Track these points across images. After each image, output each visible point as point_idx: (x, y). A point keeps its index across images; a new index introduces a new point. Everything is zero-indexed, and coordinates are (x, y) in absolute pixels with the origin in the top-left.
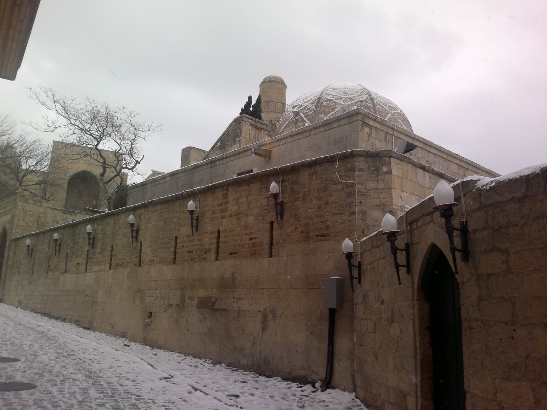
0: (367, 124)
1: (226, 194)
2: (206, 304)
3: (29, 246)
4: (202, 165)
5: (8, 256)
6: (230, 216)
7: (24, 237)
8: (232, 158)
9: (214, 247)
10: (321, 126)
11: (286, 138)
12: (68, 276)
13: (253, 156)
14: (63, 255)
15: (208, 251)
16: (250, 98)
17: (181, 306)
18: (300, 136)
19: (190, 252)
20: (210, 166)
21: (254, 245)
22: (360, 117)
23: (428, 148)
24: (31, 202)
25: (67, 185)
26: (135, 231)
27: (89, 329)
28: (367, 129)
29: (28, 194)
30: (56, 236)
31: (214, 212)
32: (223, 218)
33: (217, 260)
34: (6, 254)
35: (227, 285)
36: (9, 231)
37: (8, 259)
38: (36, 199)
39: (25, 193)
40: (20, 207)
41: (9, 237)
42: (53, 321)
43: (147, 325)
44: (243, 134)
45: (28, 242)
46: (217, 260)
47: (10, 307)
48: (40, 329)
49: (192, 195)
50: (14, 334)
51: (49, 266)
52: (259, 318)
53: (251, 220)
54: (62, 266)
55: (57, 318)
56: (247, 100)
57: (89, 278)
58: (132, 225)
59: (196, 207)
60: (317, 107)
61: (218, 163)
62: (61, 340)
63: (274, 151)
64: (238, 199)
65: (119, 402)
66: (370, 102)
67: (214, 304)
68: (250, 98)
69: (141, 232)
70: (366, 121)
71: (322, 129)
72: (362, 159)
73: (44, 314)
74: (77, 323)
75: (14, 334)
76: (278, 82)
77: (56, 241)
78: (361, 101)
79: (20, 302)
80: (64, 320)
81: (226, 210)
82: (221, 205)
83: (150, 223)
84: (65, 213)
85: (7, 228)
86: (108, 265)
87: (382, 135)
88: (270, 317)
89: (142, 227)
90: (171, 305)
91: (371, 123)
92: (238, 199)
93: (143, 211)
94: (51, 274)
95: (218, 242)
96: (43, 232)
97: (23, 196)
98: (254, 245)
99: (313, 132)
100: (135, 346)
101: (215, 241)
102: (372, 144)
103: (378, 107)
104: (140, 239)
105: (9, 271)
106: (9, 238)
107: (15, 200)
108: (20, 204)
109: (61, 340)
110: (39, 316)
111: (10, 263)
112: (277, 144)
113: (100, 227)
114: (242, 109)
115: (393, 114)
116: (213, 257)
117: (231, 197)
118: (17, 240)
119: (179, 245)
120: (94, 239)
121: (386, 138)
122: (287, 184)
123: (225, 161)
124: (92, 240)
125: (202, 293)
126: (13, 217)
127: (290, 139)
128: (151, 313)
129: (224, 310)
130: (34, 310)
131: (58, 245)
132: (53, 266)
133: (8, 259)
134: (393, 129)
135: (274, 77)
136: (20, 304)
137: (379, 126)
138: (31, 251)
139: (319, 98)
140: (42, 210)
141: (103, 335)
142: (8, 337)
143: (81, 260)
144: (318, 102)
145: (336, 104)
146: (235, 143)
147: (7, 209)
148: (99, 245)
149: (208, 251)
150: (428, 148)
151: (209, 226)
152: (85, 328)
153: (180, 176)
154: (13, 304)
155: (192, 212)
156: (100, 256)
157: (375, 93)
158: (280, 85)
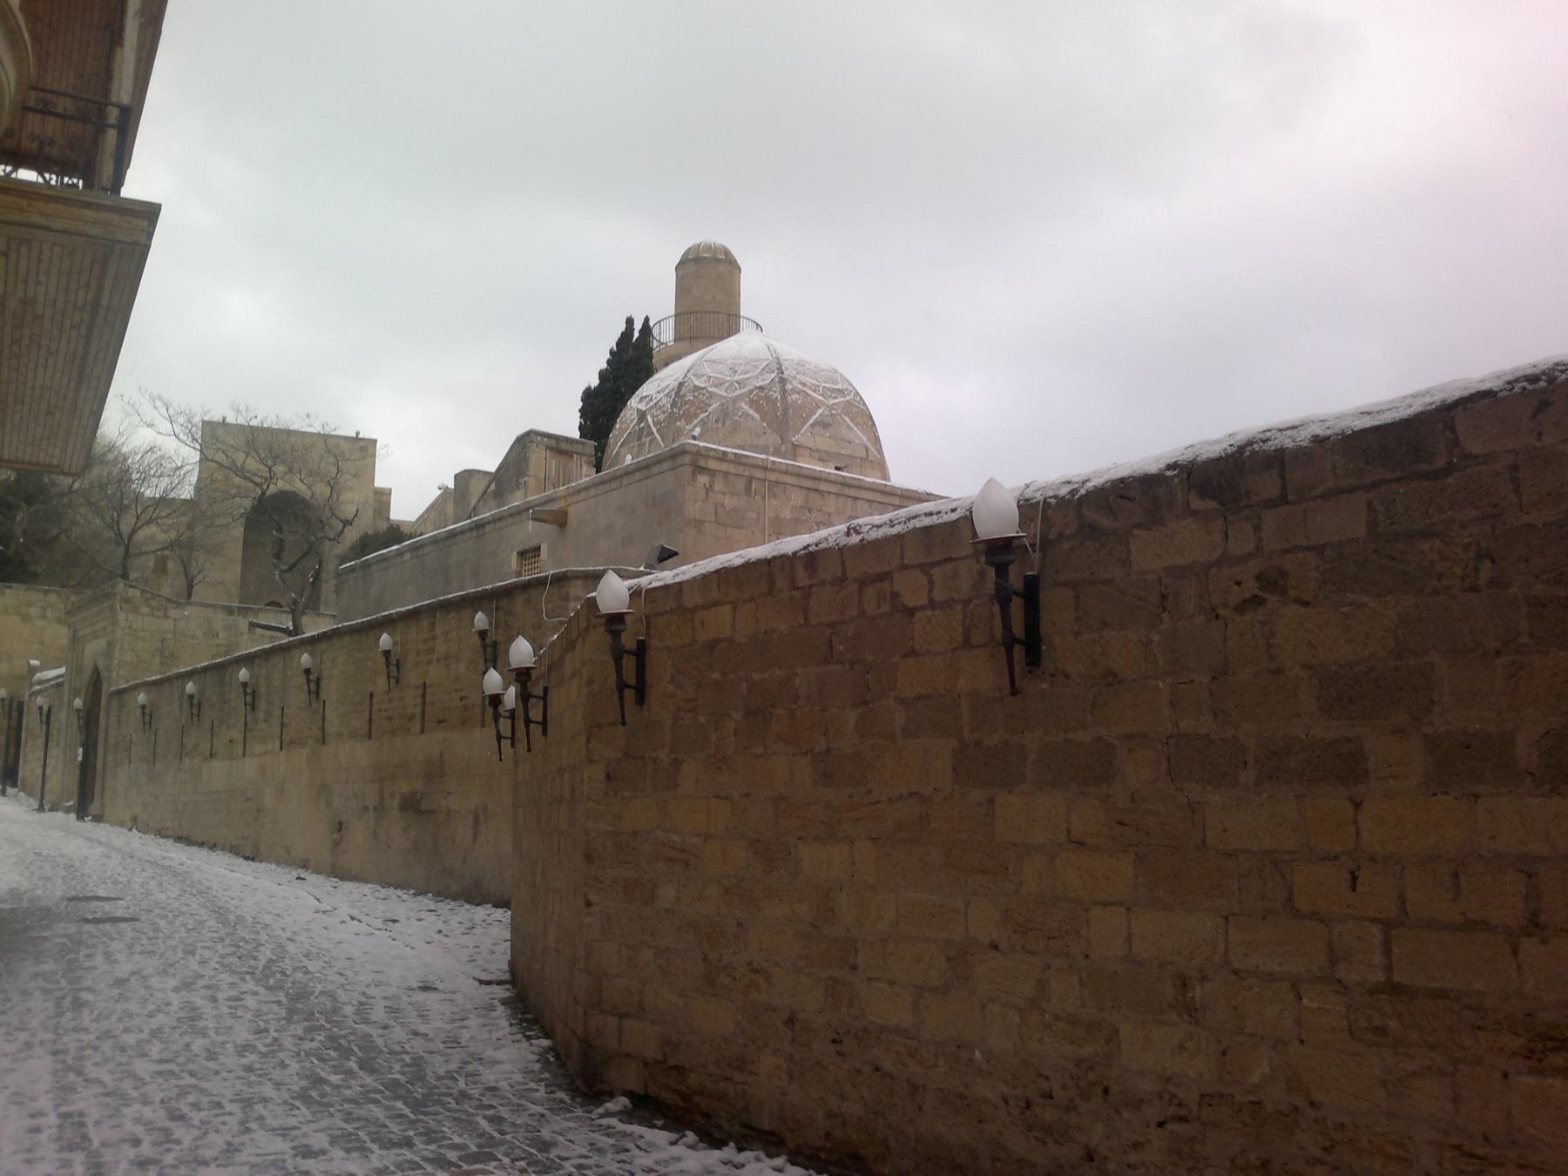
0: (704, 470)
1: (433, 624)
2: (412, 805)
3: (143, 707)
4: (462, 531)
5: (107, 725)
6: (438, 660)
7: (136, 687)
8: (510, 521)
9: (418, 710)
10: (636, 470)
11: (587, 488)
12: (216, 764)
13: (531, 525)
14: (207, 724)
15: (411, 718)
16: (630, 322)
17: (380, 809)
18: (607, 487)
19: (390, 719)
20: (475, 533)
21: (465, 708)
22: (687, 459)
23: (853, 492)
24: (145, 610)
25: (238, 531)
26: (313, 680)
27: (253, 859)
28: (703, 479)
29: (138, 593)
30: (190, 687)
31: (418, 652)
32: (429, 663)
33: (422, 732)
34: (102, 722)
35: (435, 772)
36: (104, 675)
37: (107, 732)
38: (154, 603)
39: (131, 592)
40: (123, 624)
41: (105, 686)
42: (195, 849)
43: (336, 844)
44: (532, 470)
45: (142, 698)
46: (422, 732)
47: (117, 829)
48: (167, 863)
49: (387, 623)
50: (120, 869)
51: (183, 746)
52: (470, 820)
53: (462, 667)
54: (205, 747)
55: (201, 845)
56: (623, 327)
57: (250, 766)
58: (307, 672)
59: (395, 643)
60: (674, 405)
61: (488, 528)
62: (197, 876)
63: (570, 509)
64: (447, 633)
65: (553, 1144)
66: (777, 388)
67: (419, 802)
68: (630, 322)
69: (323, 684)
70: (702, 463)
71: (638, 476)
72: (579, 582)
73: (179, 839)
74: (235, 850)
75: (120, 869)
76: (718, 261)
77: (191, 697)
78: (761, 388)
79: (135, 819)
80: (213, 847)
81: (431, 651)
82: (426, 641)
83: (337, 667)
84: (231, 613)
85: (101, 664)
86: (278, 743)
87: (740, 484)
88: (482, 817)
89: (325, 674)
90: (367, 808)
91: (713, 465)
92: (447, 633)
93: (325, 645)
94: (187, 761)
95: (424, 703)
96: (169, 679)
97: (127, 601)
98: (465, 708)
99: (625, 481)
100: (313, 879)
101: (419, 701)
102: (716, 505)
103: (795, 397)
104: (323, 695)
105: (110, 758)
106: (108, 688)
107: (112, 609)
108: (122, 616)
109: (197, 876)
110: (169, 843)
111: (111, 740)
112: (574, 499)
113: (263, 672)
114: (611, 352)
115: (831, 408)
116: (418, 728)
117: (440, 629)
118: (121, 692)
119: (375, 707)
120: (254, 694)
121: (748, 488)
122: (500, 613)
123: (498, 525)
124: (251, 695)
125: (405, 787)
126: (109, 644)
127: (593, 492)
128: (341, 824)
129: (432, 812)
130: (161, 833)
131: (195, 705)
132: (189, 746)
133: (107, 732)
134: (766, 469)
135: (708, 248)
136: (135, 823)
137: (732, 469)
138: (148, 715)
139: (681, 385)
140: (168, 625)
141: (273, 866)
142: (109, 874)
143: (237, 734)
144: (677, 394)
145: (712, 396)
146: (518, 487)
147: (98, 626)
148: (262, 705)
149: (411, 718)
150: (853, 492)
151: (412, 677)
152: (247, 858)
153: (427, 550)
154: (122, 825)
155: (387, 653)
156: (264, 725)
157: (801, 363)
158: (722, 268)
